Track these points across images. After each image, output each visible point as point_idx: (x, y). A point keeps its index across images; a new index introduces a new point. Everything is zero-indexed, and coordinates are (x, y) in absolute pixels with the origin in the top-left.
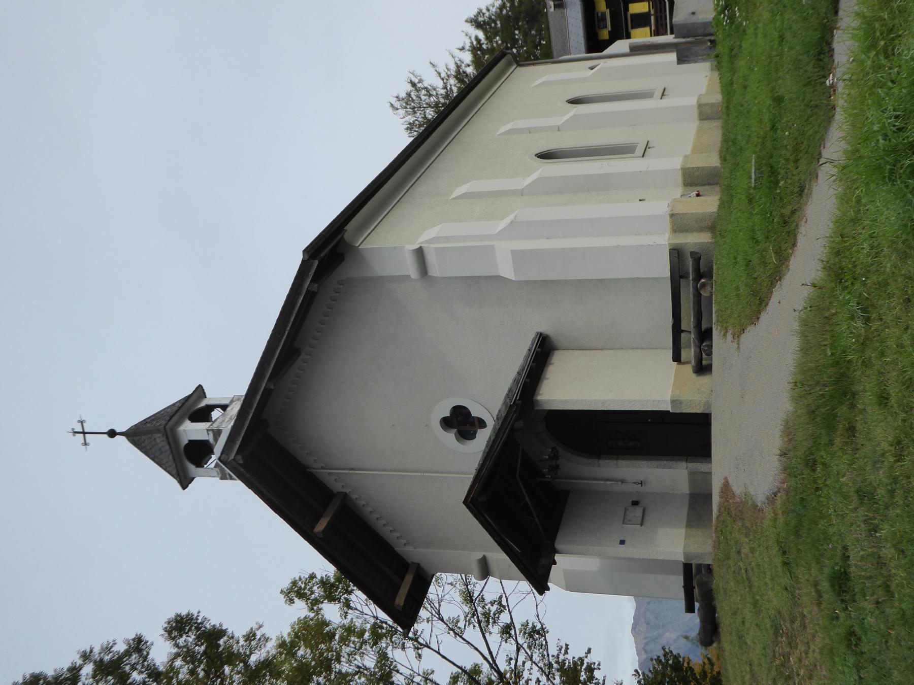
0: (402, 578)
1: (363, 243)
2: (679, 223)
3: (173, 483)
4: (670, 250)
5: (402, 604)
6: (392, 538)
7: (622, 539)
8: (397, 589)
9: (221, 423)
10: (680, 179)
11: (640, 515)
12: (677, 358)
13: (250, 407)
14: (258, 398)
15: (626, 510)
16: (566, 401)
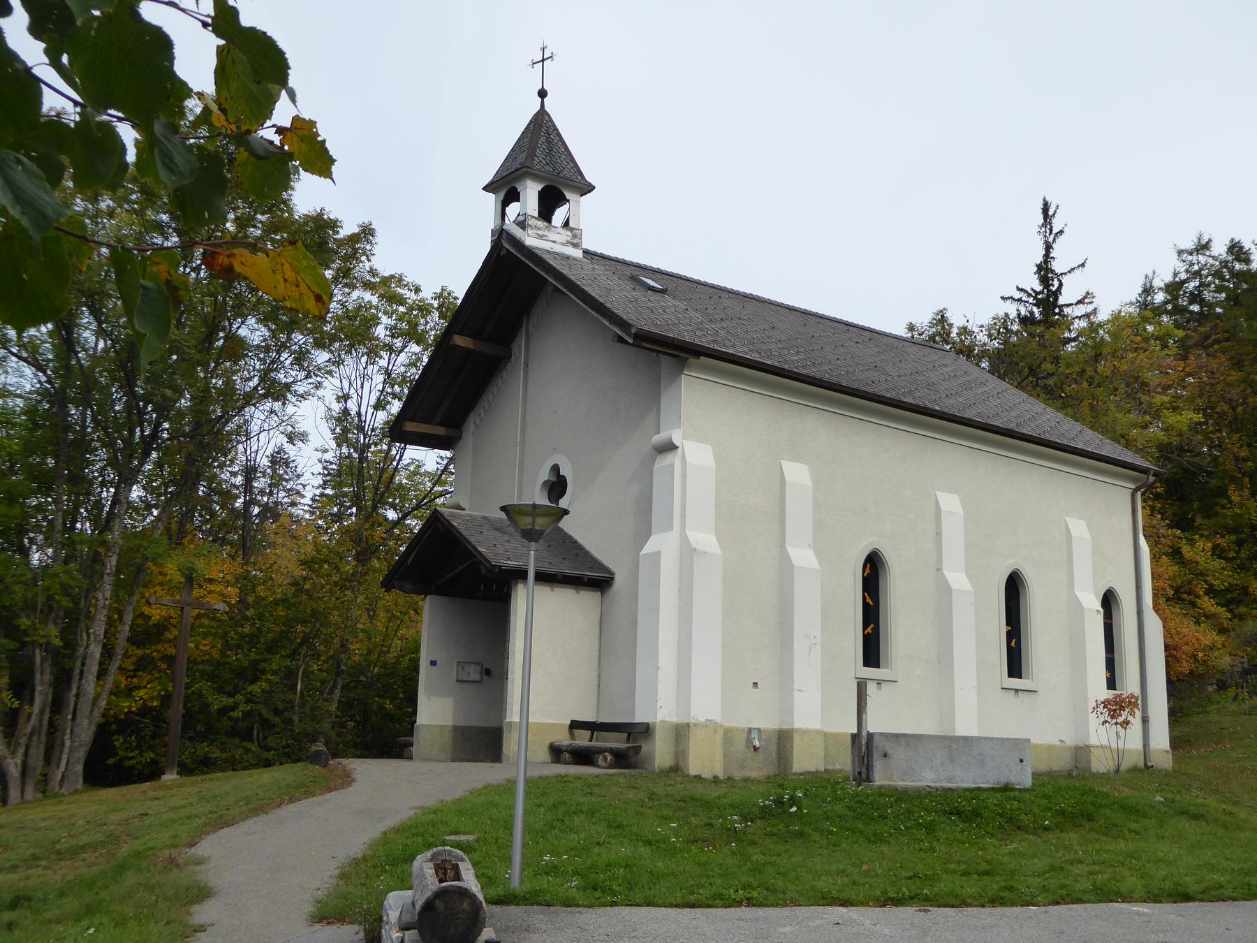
0: (440, 424)
1: (754, 357)
2: (681, 732)
3: (488, 178)
4: (648, 724)
5: (407, 429)
6: (479, 410)
7: (438, 663)
8: (427, 421)
9: (536, 227)
10: (785, 727)
11: (471, 679)
12: (575, 725)
13: (537, 265)
14: (542, 274)
15: (478, 664)
16: (516, 614)
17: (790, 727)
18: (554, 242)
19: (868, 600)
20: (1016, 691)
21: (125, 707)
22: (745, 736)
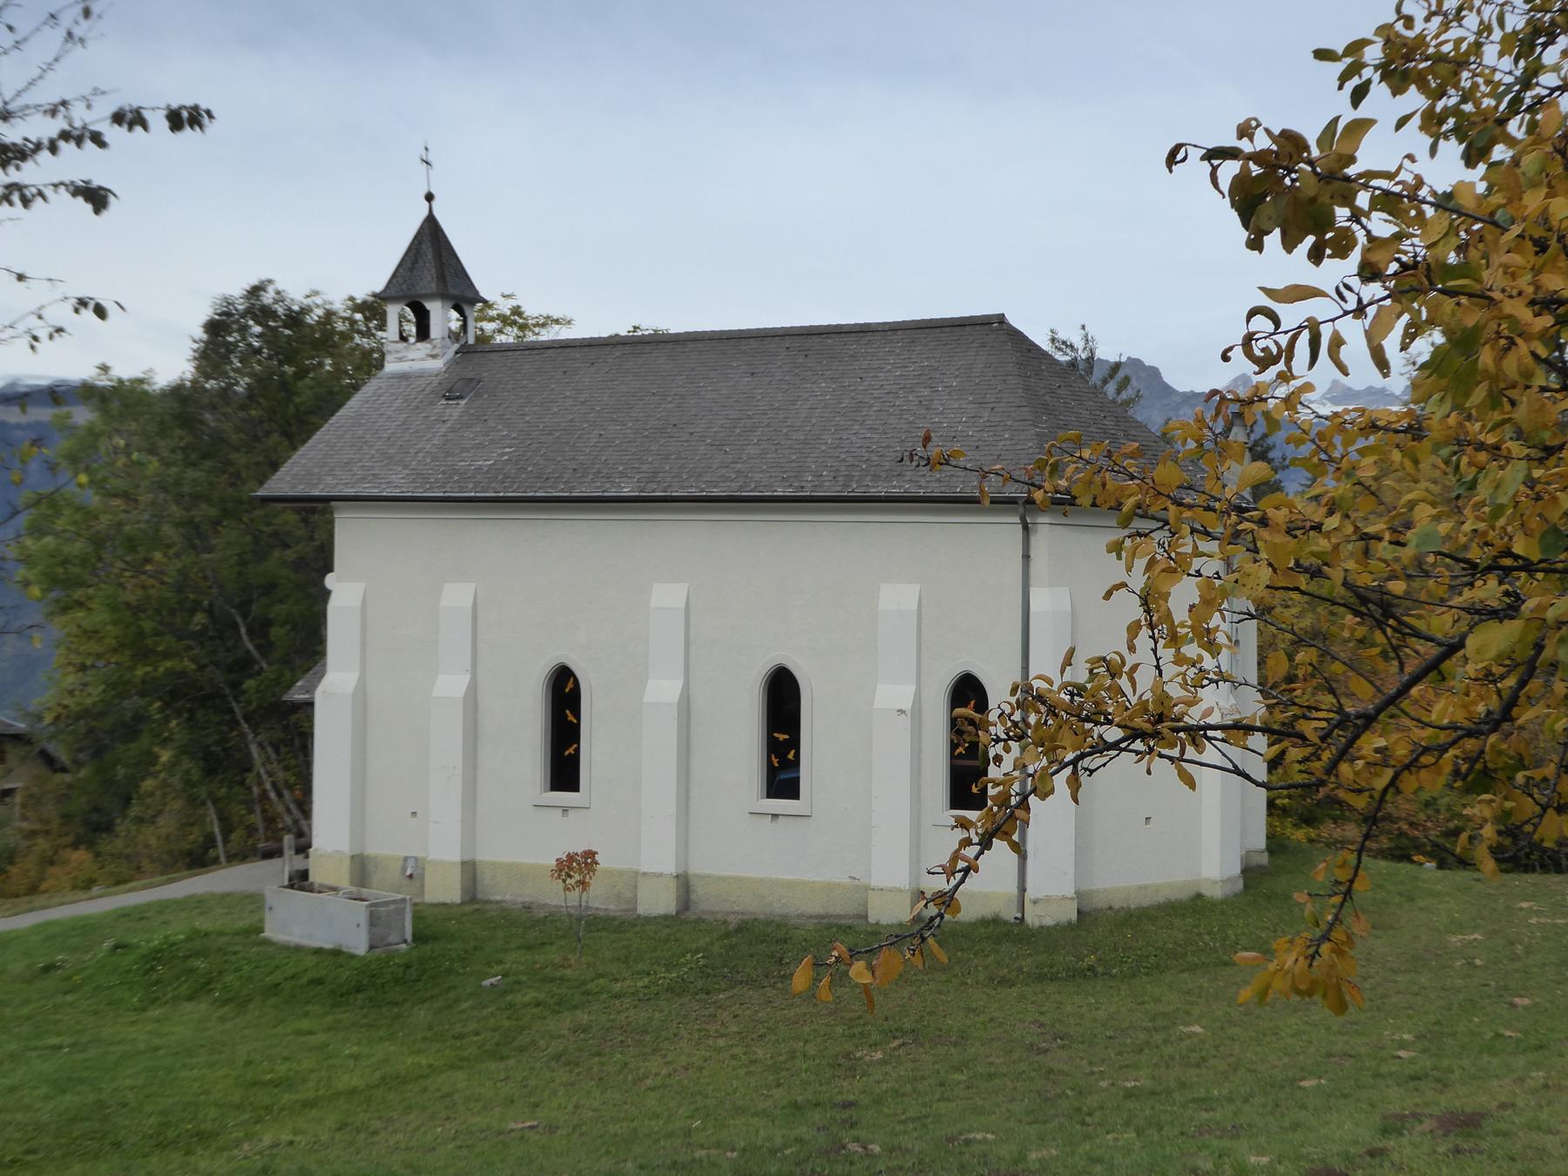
17: (347, 862)
18: (413, 360)
19: (571, 718)
20: (775, 816)
21: (284, 821)
22: (400, 863)
